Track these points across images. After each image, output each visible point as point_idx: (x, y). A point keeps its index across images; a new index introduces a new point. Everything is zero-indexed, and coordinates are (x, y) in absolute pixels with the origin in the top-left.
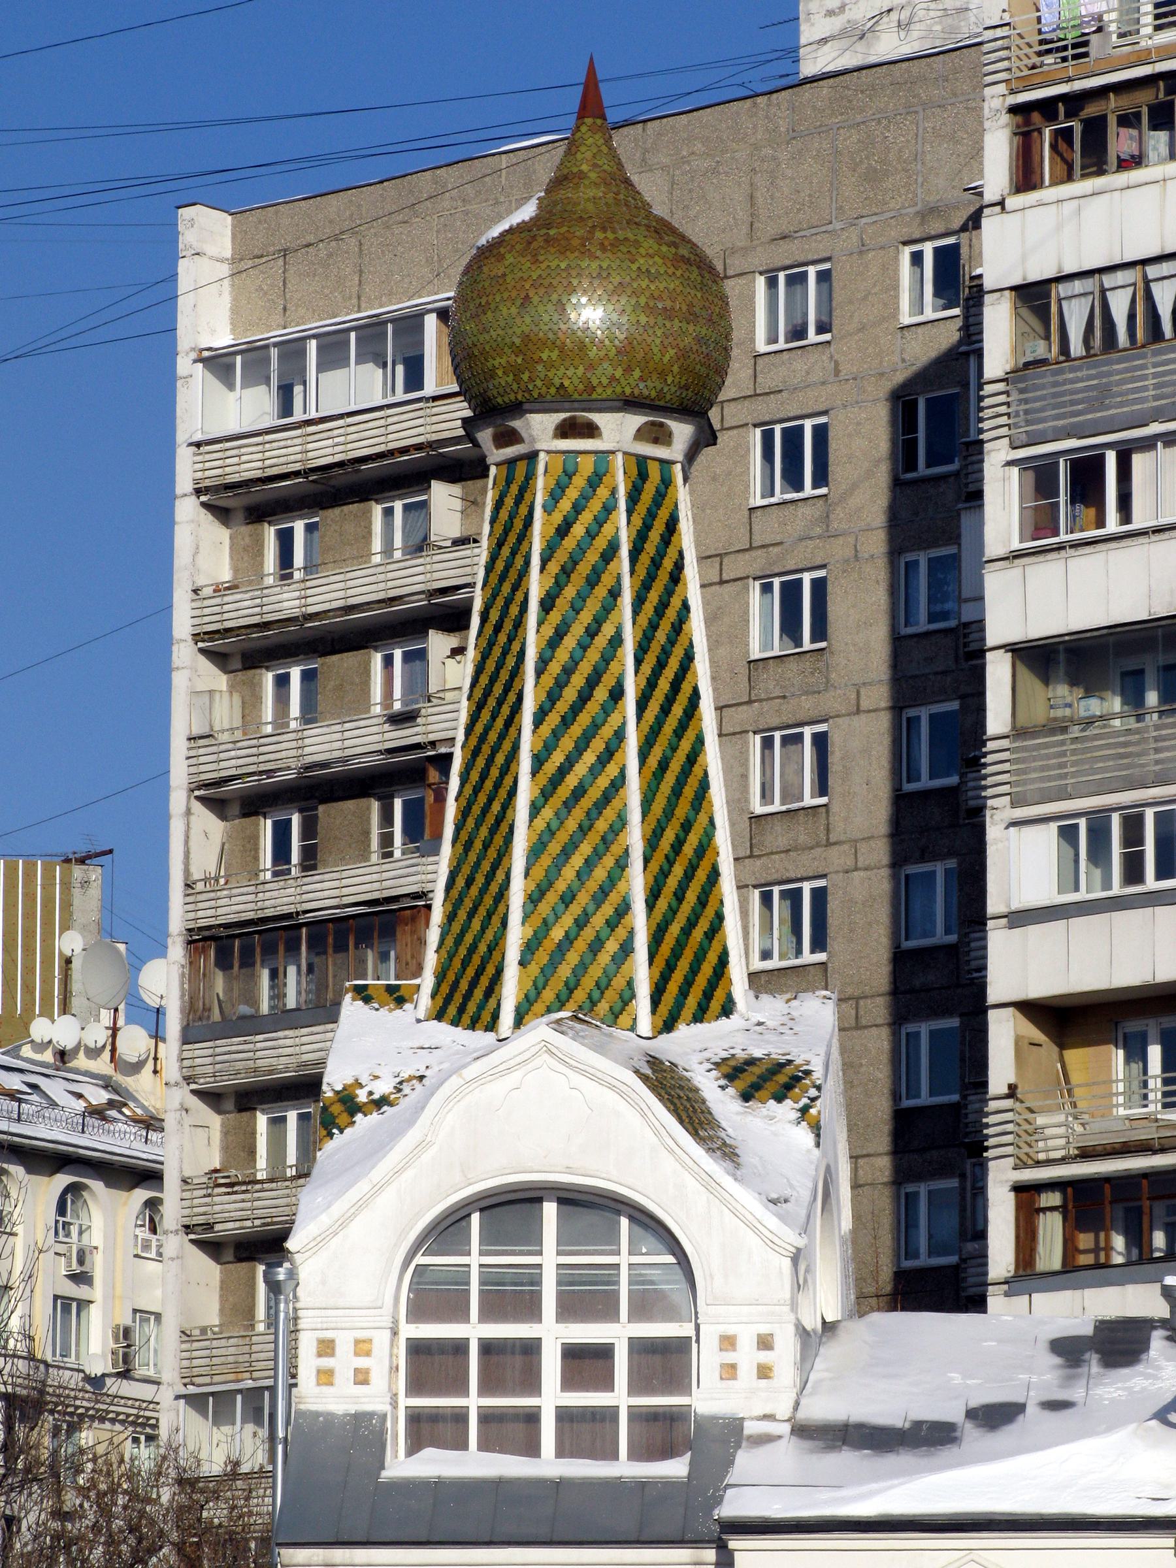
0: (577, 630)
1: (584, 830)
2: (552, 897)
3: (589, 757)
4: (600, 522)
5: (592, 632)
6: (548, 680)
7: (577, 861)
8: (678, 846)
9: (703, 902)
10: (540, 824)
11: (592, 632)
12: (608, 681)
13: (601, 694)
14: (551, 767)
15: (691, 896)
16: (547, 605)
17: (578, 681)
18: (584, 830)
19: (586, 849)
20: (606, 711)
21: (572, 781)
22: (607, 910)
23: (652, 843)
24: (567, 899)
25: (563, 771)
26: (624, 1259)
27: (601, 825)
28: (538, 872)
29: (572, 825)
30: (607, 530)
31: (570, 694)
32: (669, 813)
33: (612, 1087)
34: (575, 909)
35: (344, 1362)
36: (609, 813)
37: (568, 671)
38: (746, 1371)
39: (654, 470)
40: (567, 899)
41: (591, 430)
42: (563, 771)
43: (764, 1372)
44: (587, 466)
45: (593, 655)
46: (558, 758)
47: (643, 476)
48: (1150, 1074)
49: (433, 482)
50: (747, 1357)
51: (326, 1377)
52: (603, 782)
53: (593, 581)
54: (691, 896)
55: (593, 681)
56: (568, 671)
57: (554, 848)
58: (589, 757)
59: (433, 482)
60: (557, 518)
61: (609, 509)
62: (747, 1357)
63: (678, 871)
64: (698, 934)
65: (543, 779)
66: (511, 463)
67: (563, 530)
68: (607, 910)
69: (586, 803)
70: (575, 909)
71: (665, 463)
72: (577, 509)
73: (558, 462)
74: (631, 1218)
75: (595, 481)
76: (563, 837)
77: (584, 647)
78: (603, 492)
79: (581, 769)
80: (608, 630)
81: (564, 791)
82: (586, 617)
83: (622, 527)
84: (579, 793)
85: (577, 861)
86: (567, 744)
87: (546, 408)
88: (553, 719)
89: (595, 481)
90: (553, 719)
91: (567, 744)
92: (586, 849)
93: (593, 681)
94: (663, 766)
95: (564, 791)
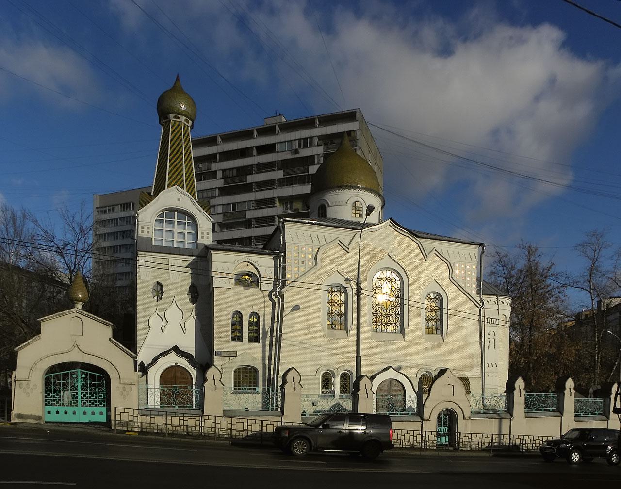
0: (176, 144)
1: (176, 171)
2: (172, 179)
3: (177, 161)
4: (179, 131)
5: (178, 145)
6: (172, 150)
7: (176, 174)
8: (189, 176)
9: (192, 184)
10: (170, 169)
11: (178, 145)
12: (180, 151)
13: (179, 153)
14: (172, 162)
15: (191, 183)
16: (171, 140)
17: (176, 151)
18: (176, 171)
19: (177, 173)
20: (180, 155)
21: (175, 164)
22: (180, 181)
23: (186, 174)
24: (174, 179)
25: (174, 163)
26: (96, 383)
27: (179, 170)
28: (170, 175)
29: (175, 169)
30: (180, 132)
31: (175, 152)
32: (188, 171)
33: (185, 195)
34: (175, 181)
35: (145, 230)
36: (180, 169)
37: (175, 149)
38: (205, 237)
39: (186, 126)
40: (174, 179)
41: (179, 118)
42: (174, 163)
43: (208, 238)
44: (177, 123)
45: (178, 148)
46: (173, 160)
47: (185, 126)
48: (256, 193)
49: (105, 421)
50: (205, 235)
51: (143, 232)
52: (179, 165)
53: (178, 138)
54: (191, 183)
55: (178, 151)
56: (175, 149)
57: (172, 172)
58: (177, 161)
59: (105, 421)
60: (173, 129)
61: (181, 129)
62: (205, 235)
63: (189, 179)
64: (192, 188)
65: (171, 163)
66: (166, 122)
67: (174, 131)
68: (180, 181)
69: (177, 167)
70: (175, 181)
71: (188, 126)
72: (176, 128)
73: (173, 122)
74: (188, 217)
75: (179, 125)
76: (173, 171)
77: (177, 146)
78: (180, 127)
79: (176, 162)
80: (180, 145)
81: (174, 165)
82: (177, 143)
84: (176, 165)
85: (176, 174)
86: (174, 159)
87: (172, 114)
88: (172, 155)
89: (179, 125)
90: (172, 155)
91: (174, 159)
92: (177, 173)
93: (178, 151)
94: (187, 164)
95: (174, 165)
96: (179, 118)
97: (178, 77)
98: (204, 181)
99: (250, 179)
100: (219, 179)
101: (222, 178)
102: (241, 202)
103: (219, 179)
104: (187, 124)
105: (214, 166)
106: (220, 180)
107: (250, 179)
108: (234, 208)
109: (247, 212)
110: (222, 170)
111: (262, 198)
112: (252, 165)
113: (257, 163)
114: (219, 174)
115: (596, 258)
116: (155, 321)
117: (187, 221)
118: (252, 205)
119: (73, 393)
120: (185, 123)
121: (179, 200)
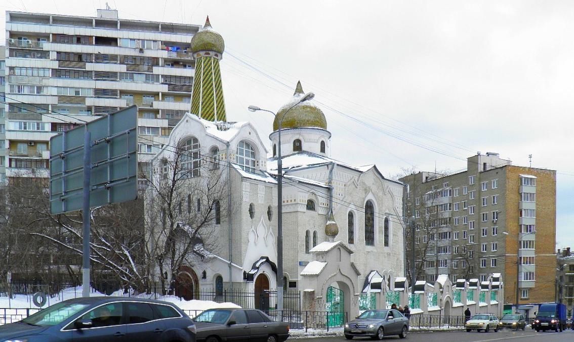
41: (209, 54)
44: (209, 58)
83: (213, 71)
96: (209, 54)
97: (208, 20)
98: (15, 58)
99: (89, 67)
100: (52, 60)
101: (57, 60)
102: (67, 87)
103: (52, 60)
104: (217, 57)
105: (46, 46)
106: (53, 62)
107: (89, 67)
108: (77, 93)
109: (86, 99)
110: (58, 52)
111: (103, 87)
112: (92, 54)
113: (97, 53)
114: (53, 55)
115: (144, 137)
116: (252, 237)
117: (244, 149)
118: (92, 93)
119: (329, 296)
120: (215, 57)
121: (250, 133)
